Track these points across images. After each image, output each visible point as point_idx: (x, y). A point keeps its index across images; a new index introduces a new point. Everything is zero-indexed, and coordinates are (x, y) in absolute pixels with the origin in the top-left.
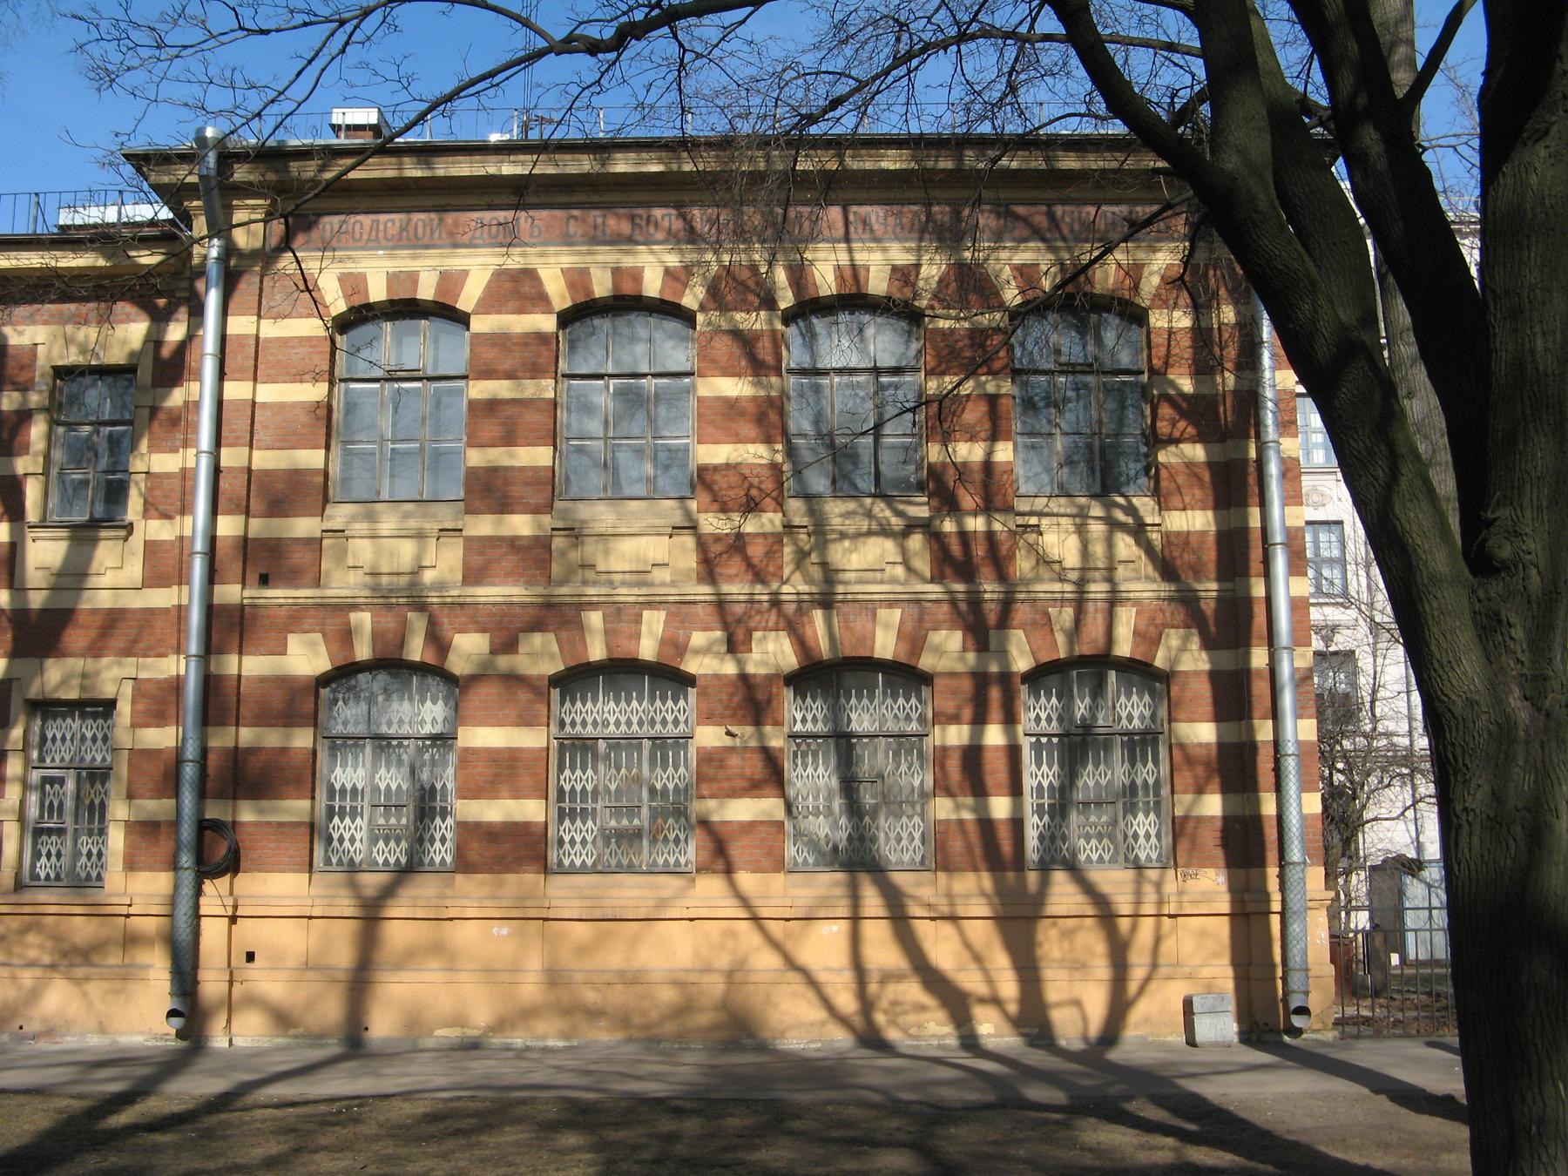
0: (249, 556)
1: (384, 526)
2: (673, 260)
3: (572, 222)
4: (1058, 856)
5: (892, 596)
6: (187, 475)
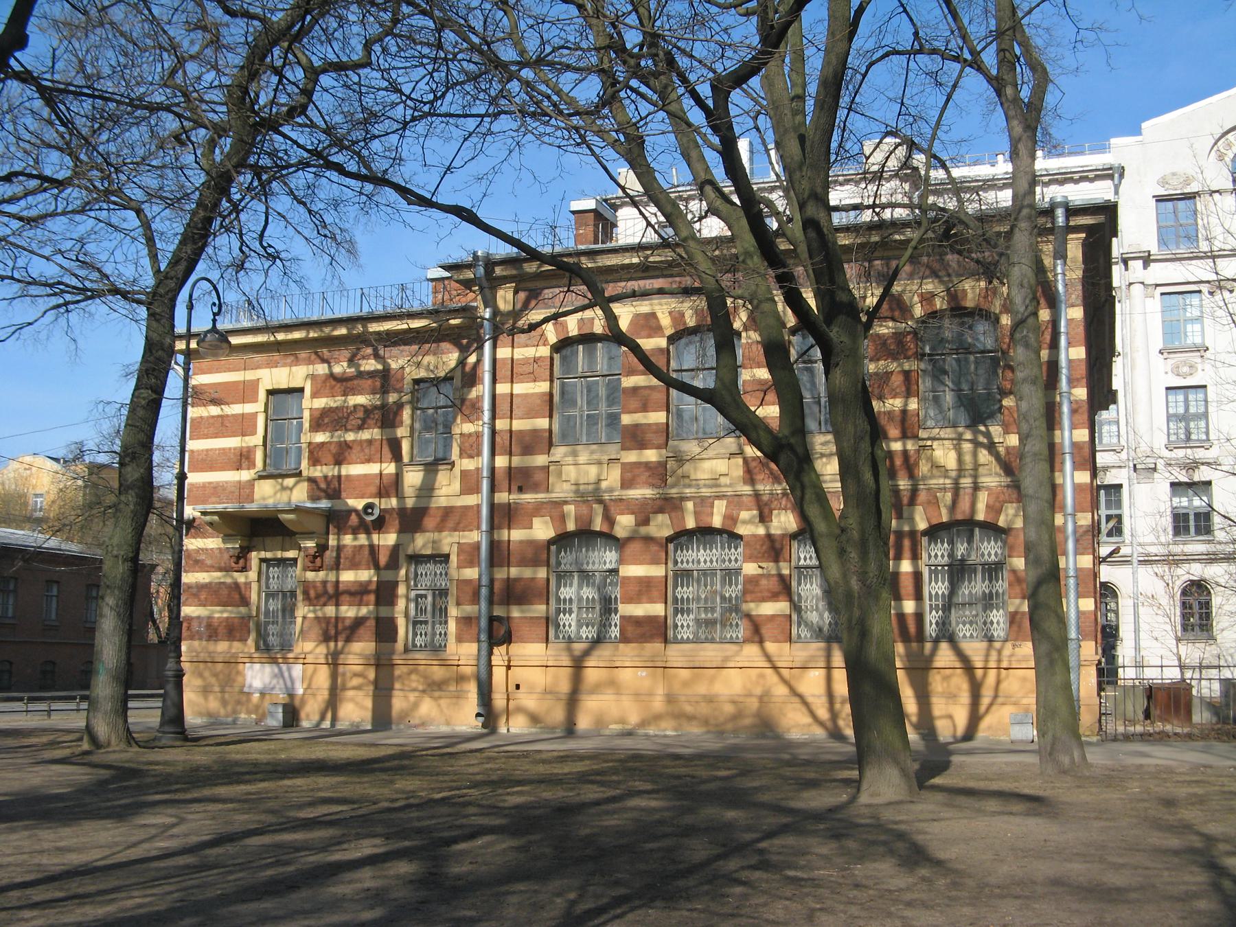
4: (947, 635)
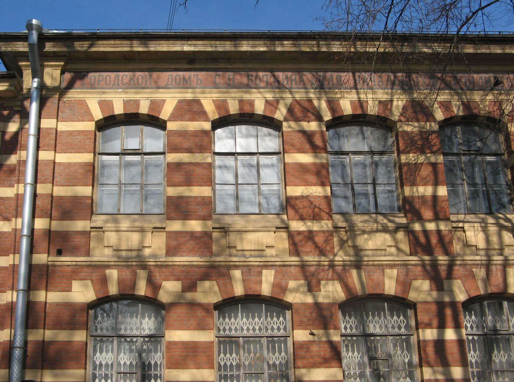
0: (51, 240)
1: (124, 225)
2: (269, 96)
3: (217, 77)
5: (392, 262)
6: (19, 198)
